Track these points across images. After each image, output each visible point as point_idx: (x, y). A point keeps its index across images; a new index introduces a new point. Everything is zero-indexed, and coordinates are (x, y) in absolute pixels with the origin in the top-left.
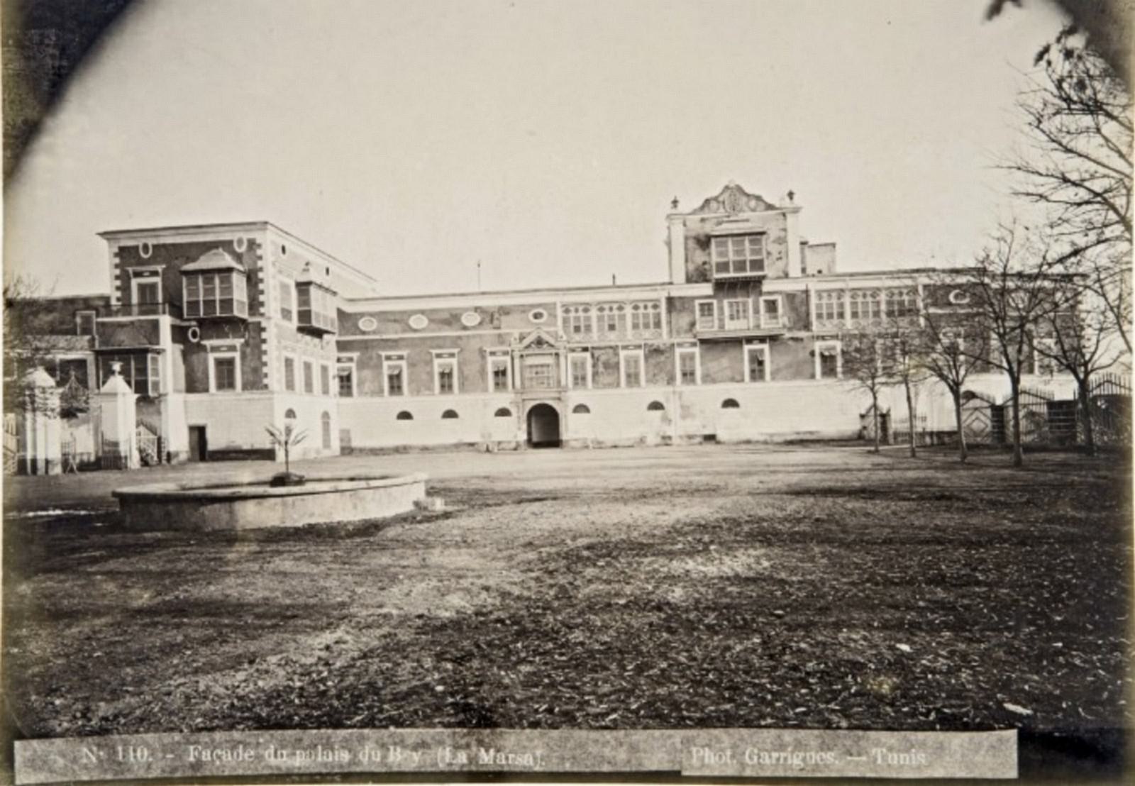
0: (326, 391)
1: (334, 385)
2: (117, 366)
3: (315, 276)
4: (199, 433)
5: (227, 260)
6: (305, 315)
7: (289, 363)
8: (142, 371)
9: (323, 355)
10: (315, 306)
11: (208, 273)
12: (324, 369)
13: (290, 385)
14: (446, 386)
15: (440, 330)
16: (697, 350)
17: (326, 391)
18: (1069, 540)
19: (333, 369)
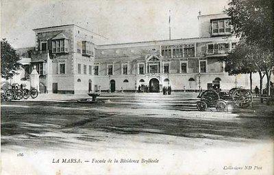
0: (90, 73)
1: (93, 71)
2: (35, 67)
3: (88, 39)
4: (55, 85)
5: (64, 36)
6: (84, 51)
7: (79, 65)
8: (42, 68)
9: (90, 62)
10: (87, 49)
11: (59, 40)
12: (90, 67)
13: (79, 72)
14: (125, 72)
15: (76, 107)
16: (206, 61)
17: (90, 73)
18: (222, 30)
19: (93, 66)
